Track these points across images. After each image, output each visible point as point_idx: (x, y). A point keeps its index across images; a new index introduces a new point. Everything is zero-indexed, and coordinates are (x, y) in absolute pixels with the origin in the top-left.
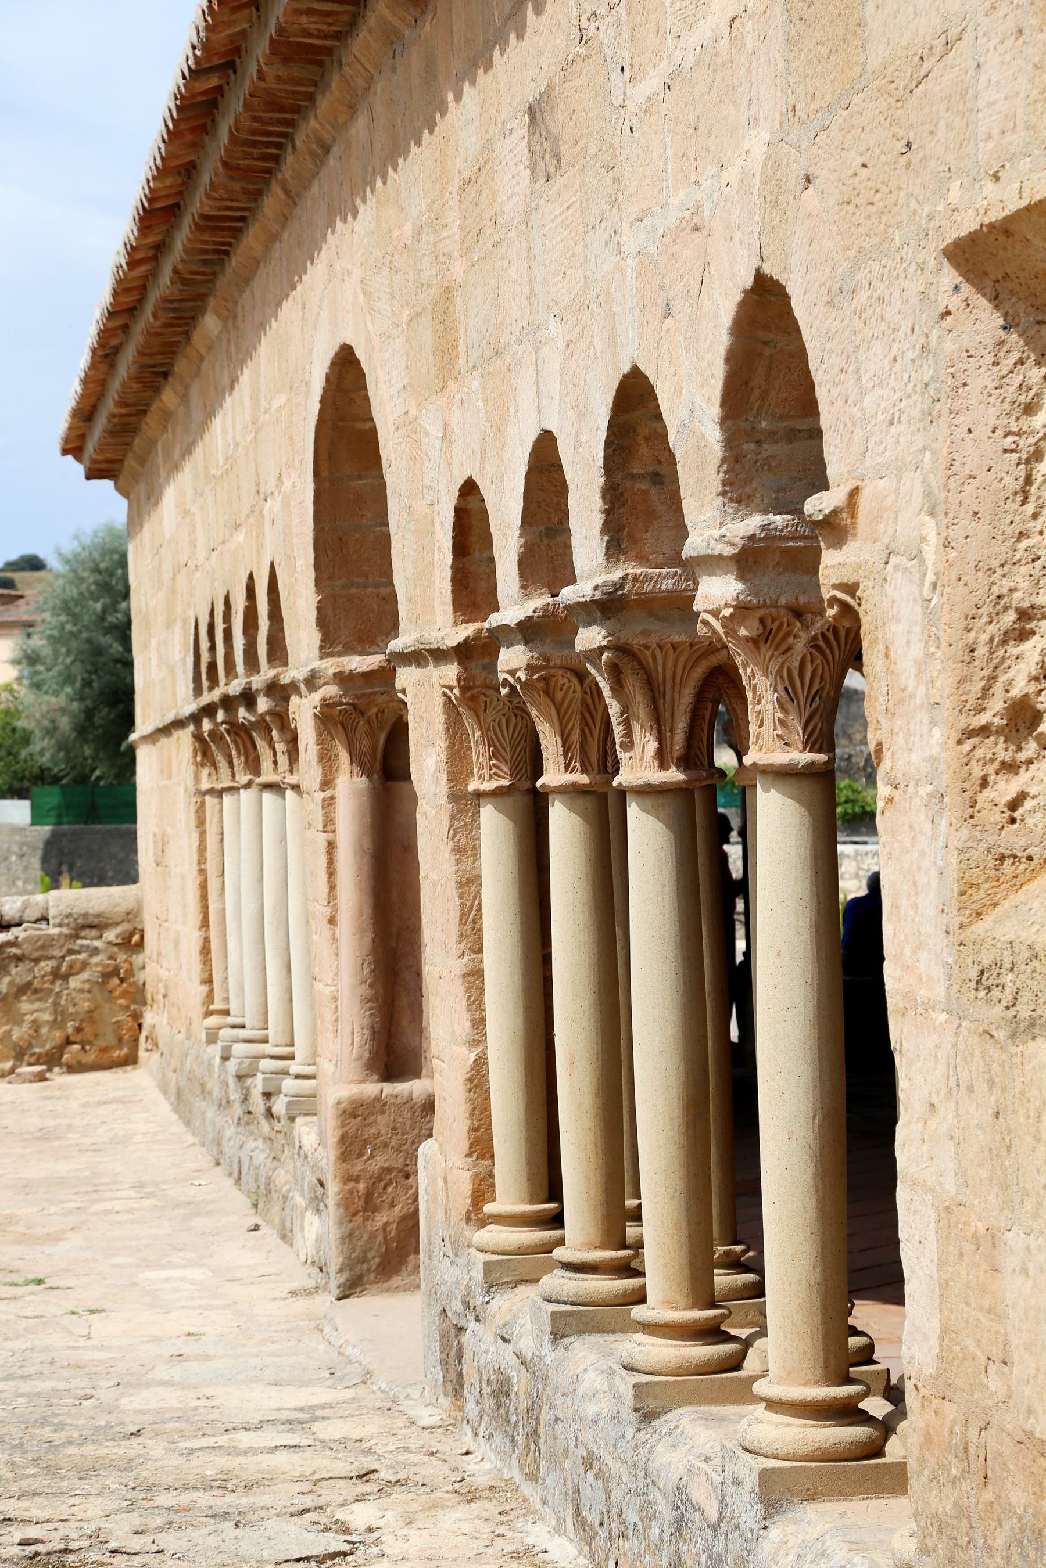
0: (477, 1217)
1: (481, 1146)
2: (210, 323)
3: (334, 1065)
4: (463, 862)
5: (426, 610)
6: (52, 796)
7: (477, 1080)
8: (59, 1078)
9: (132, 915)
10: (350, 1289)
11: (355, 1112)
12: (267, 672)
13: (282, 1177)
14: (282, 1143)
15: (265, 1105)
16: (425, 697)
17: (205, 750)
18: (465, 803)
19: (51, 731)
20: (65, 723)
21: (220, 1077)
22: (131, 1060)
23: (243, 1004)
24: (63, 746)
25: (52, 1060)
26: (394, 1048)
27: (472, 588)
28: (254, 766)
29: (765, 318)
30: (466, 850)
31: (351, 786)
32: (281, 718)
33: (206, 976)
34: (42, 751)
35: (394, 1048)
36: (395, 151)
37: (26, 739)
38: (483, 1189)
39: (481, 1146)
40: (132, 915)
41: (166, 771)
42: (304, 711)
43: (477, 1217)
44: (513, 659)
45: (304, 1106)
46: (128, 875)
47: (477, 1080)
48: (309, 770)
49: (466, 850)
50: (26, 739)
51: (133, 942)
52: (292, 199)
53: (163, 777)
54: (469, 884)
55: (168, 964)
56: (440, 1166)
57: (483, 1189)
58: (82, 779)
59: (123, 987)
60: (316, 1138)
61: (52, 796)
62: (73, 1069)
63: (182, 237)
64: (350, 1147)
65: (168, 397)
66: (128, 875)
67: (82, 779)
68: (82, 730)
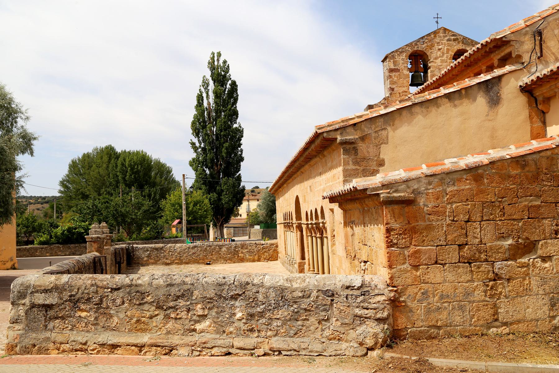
0: (309, 271)
1: (309, 265)
2: (285, 185)
3: (298, 259)
4: (307, 241)
5: (304, 221)
6: (263, 225)
7: (309, 259)
8: (269, 262)
9: (277, 243)
10: (212, 67)
11: (300, 263)
12: (291, 221)
13: (293, 270)
14: (293, 267)
15: (292, 264)
16: (304, 227)
17: (285, 227)
18: (307, 236)
19: (262, 216)
20: (264, 215)
21: (287, 261)
22: (277, 260)
23: (289, 253)
24: (264, 218)
25: (268, 260)
26: (303, 258)
27: (307, 220)
28: (290, 229)
29: (322, 207)
30: (308, 240)
31: (299, 233)
32: (292, 226)
33: (136, 349)
34: (261, 218)
35: (303, 258)
36: (301, 182)
37: (259, 217)
38: (309, 268)
39: (309, 265)
40: (277, 243)
41: (281, 228)
42: (294, 226)
43: (309, 271)
44: (310, 226)
45: (295, 263)
46: (276, 238)
47: (309, 259)
48: (295, 232)
49: (308, 240)
50: (259, 217)
51: (277, 246)
52: (293, 180)
53: (280, 229)
54: (308, 243)
55: (281, 249)
56: (306, 267)
57: (309, 268)
58: (267, 222)
59: (276, 252)
60: (296, 266)
61: (263, 225)
62: (271, 261)
63: (282, 180)
64: (299, 266)
65: (281, 189)
66: (276, 238)
67: (267, 222)
68: (267, 215)
